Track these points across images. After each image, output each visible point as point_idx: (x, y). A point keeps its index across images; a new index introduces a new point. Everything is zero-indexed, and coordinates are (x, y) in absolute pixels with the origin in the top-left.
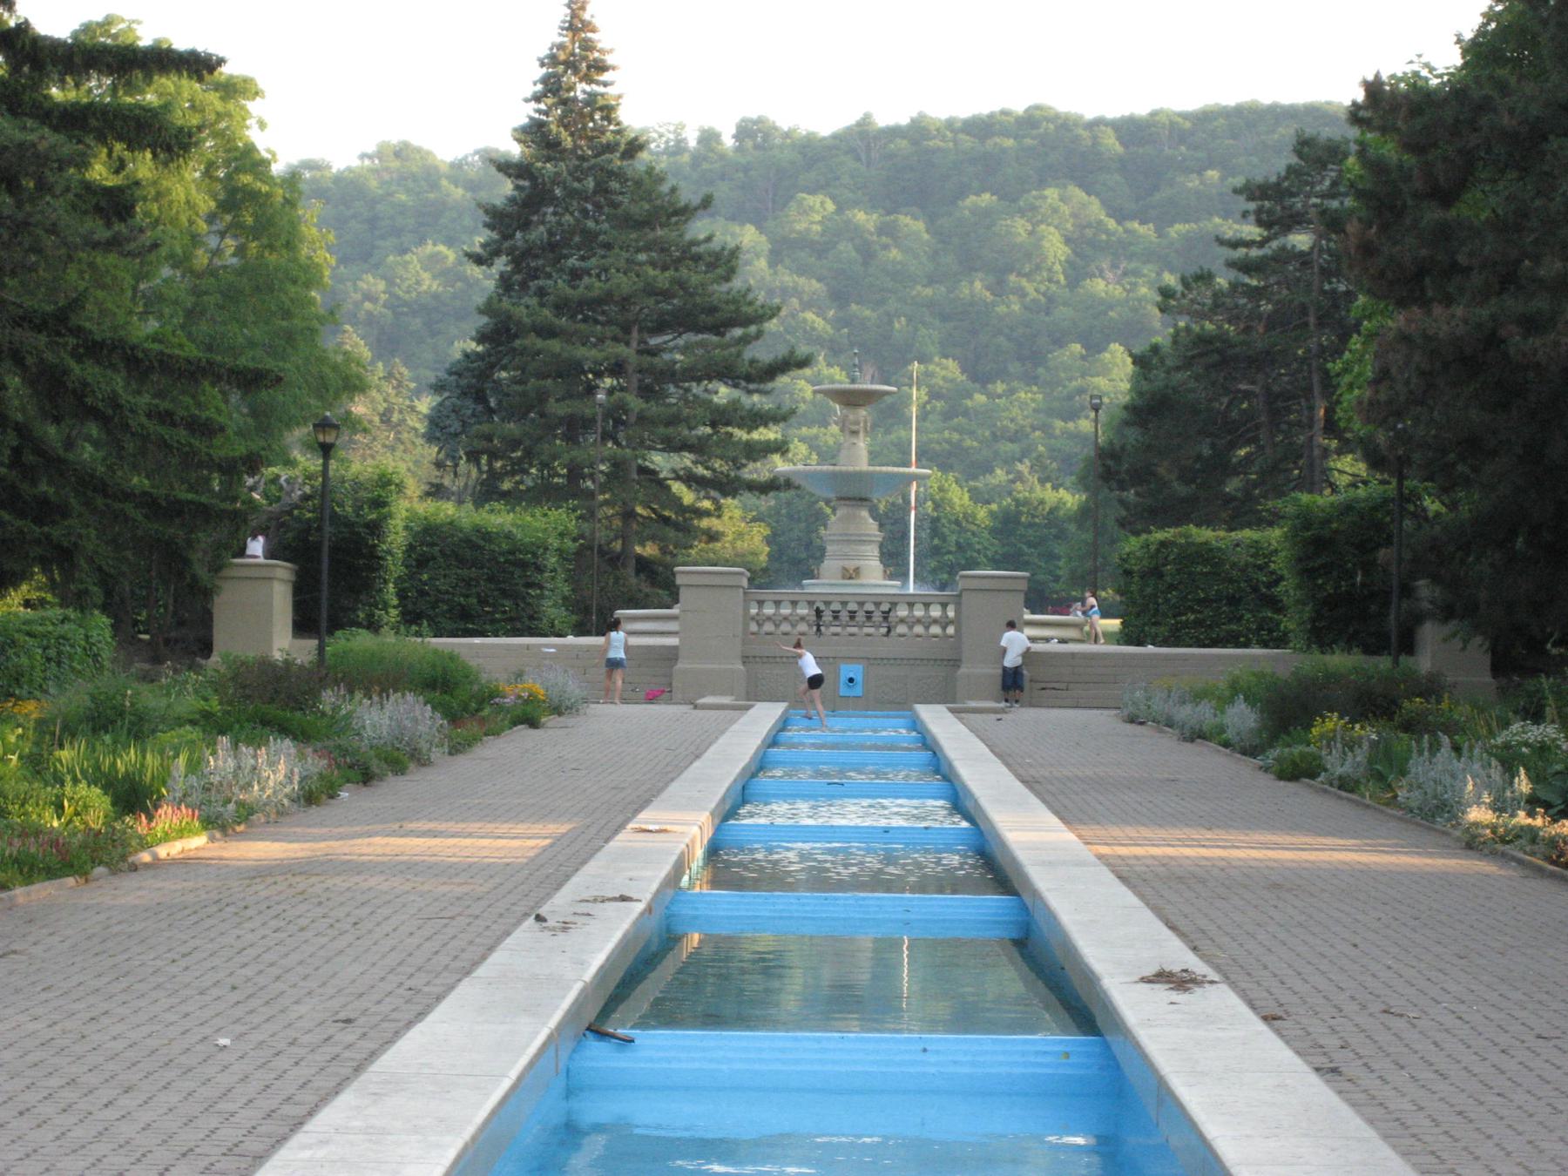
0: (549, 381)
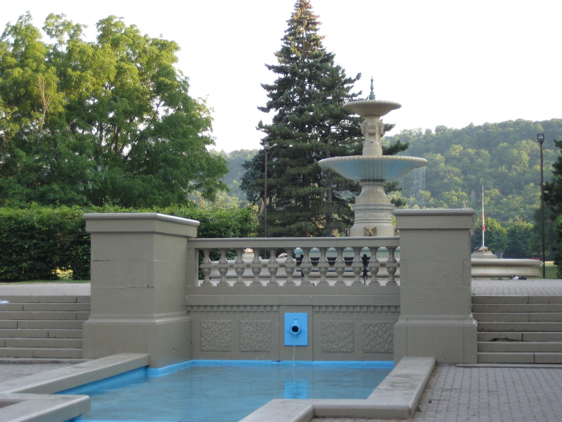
0: (288, 159)
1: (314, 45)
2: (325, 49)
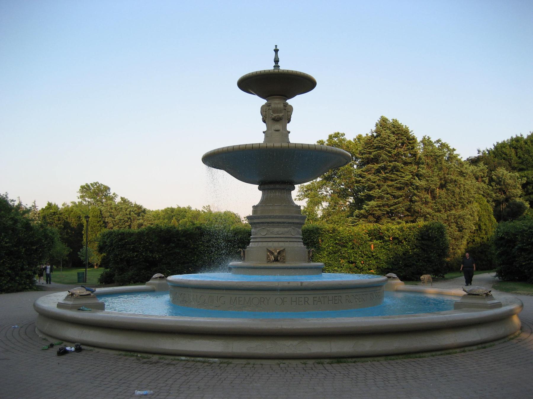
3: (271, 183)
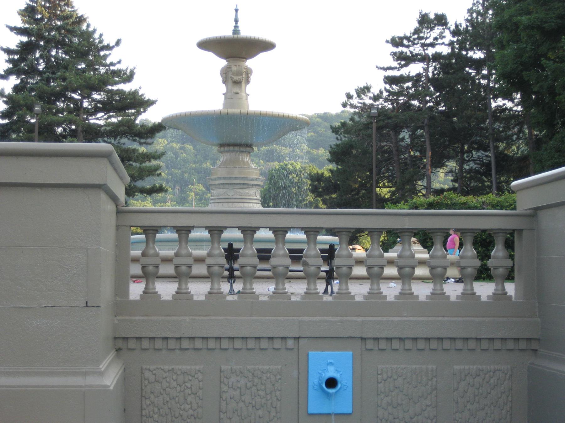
1: (65, 5)
2: (76, 10)
3: (229, 145)
